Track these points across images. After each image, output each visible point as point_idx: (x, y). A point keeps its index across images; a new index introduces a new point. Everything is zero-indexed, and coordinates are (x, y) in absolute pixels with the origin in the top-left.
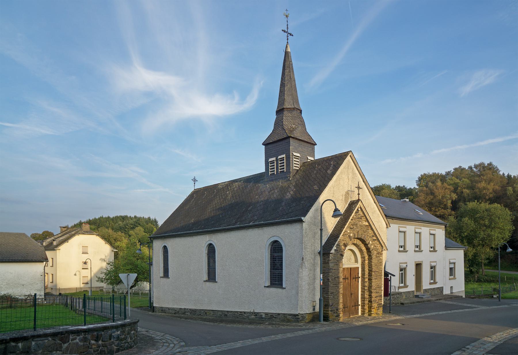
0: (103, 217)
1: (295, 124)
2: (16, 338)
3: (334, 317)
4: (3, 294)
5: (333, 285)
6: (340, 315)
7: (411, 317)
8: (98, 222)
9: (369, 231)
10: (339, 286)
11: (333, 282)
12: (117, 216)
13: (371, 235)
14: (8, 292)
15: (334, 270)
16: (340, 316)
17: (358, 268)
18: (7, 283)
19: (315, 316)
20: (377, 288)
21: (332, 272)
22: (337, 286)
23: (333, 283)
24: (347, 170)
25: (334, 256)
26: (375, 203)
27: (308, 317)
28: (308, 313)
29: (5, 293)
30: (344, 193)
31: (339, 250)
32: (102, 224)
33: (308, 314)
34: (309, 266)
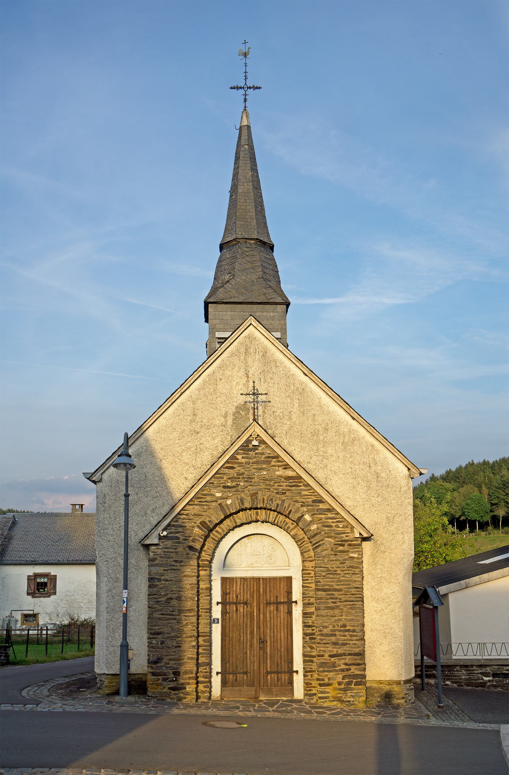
0: (473, 464)
1: (231, 271)
2: (442, 727)
3: (165, 690)
4: (83, 619)
5: (160, 616)
6: (187, 687)
7: (478, 726)
8: (462, 475)
9: (302, 490)
10: (183, 618)
11: (160, 608)
12: (503, 459)
13: (310, 500)
14: (91, 615)
15: (163, 582)
16: (187, 689)
17: (289, 580)
18: (88, 599)
19: (133, 683)
20: (337, 633)
21: (157, 585)
22: (175, 619)
23: (161, 610)
24: (242, 358)
25: (166, 550)
26: (354, 419)
27: (110, 683)
28: (107, 673)
29: (86, 618)
30: (232, 410)
31: (181, 538)
32: (469, 479)
33: (110, 676)
34: (110, 571)
